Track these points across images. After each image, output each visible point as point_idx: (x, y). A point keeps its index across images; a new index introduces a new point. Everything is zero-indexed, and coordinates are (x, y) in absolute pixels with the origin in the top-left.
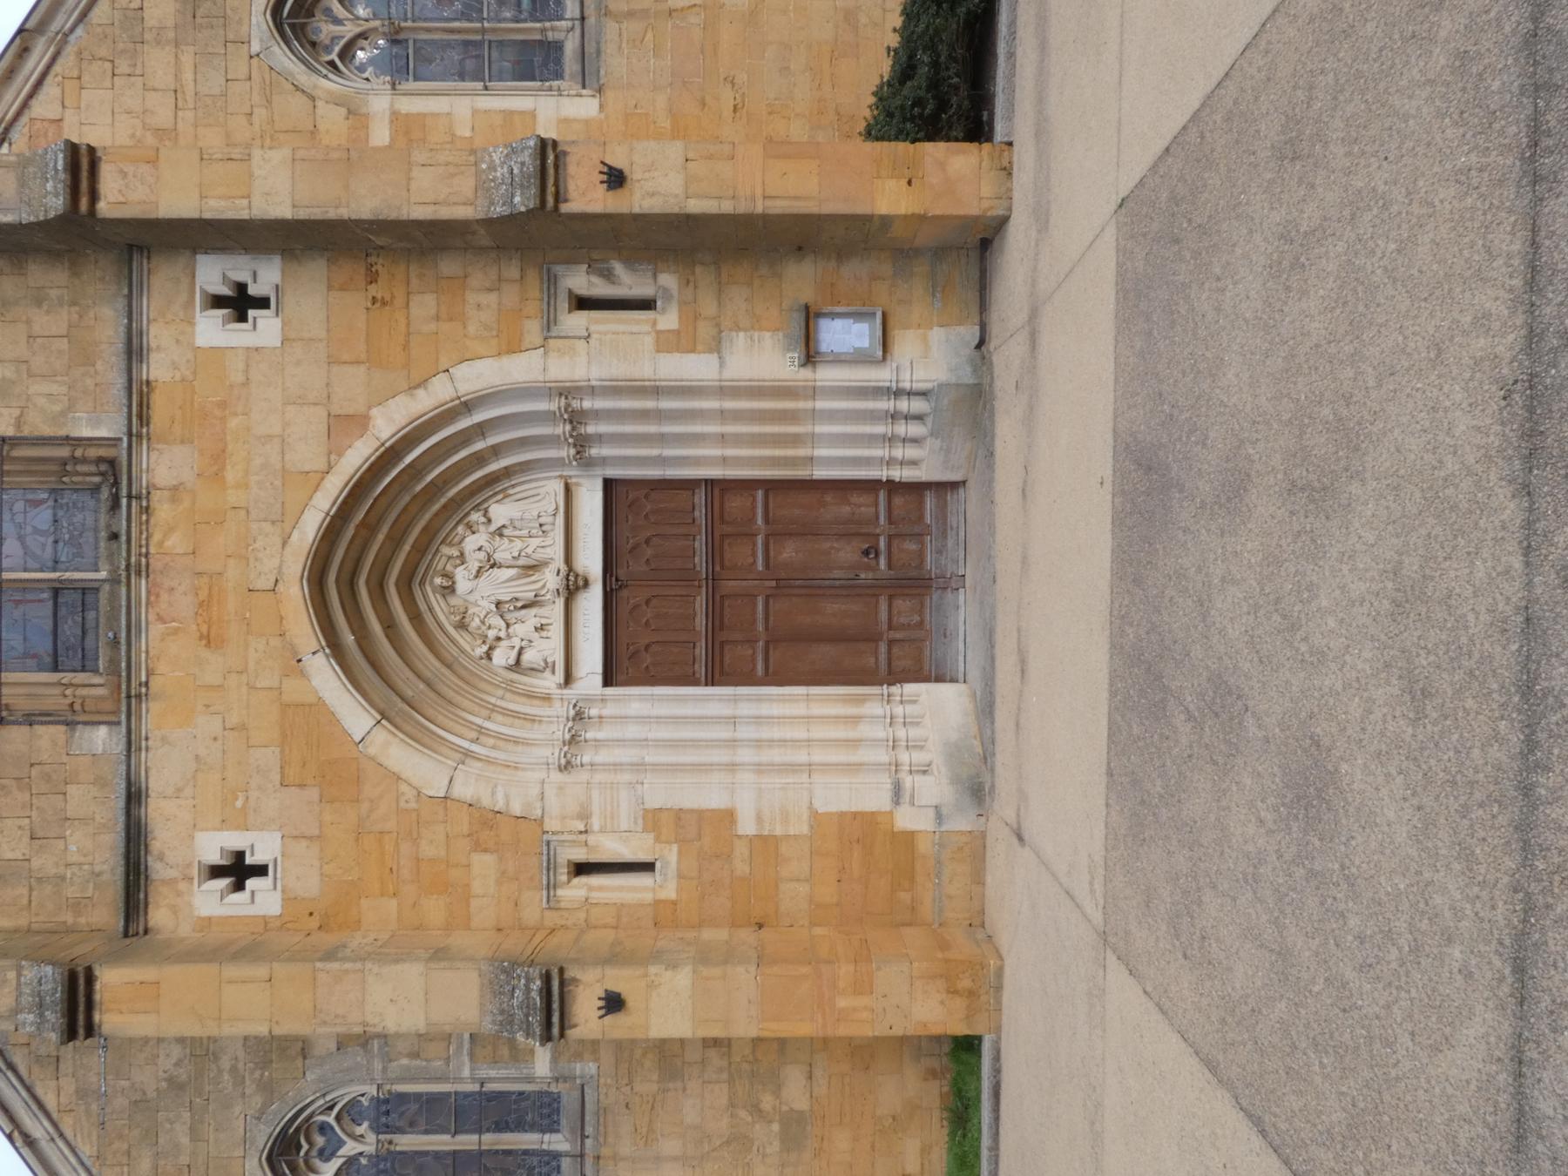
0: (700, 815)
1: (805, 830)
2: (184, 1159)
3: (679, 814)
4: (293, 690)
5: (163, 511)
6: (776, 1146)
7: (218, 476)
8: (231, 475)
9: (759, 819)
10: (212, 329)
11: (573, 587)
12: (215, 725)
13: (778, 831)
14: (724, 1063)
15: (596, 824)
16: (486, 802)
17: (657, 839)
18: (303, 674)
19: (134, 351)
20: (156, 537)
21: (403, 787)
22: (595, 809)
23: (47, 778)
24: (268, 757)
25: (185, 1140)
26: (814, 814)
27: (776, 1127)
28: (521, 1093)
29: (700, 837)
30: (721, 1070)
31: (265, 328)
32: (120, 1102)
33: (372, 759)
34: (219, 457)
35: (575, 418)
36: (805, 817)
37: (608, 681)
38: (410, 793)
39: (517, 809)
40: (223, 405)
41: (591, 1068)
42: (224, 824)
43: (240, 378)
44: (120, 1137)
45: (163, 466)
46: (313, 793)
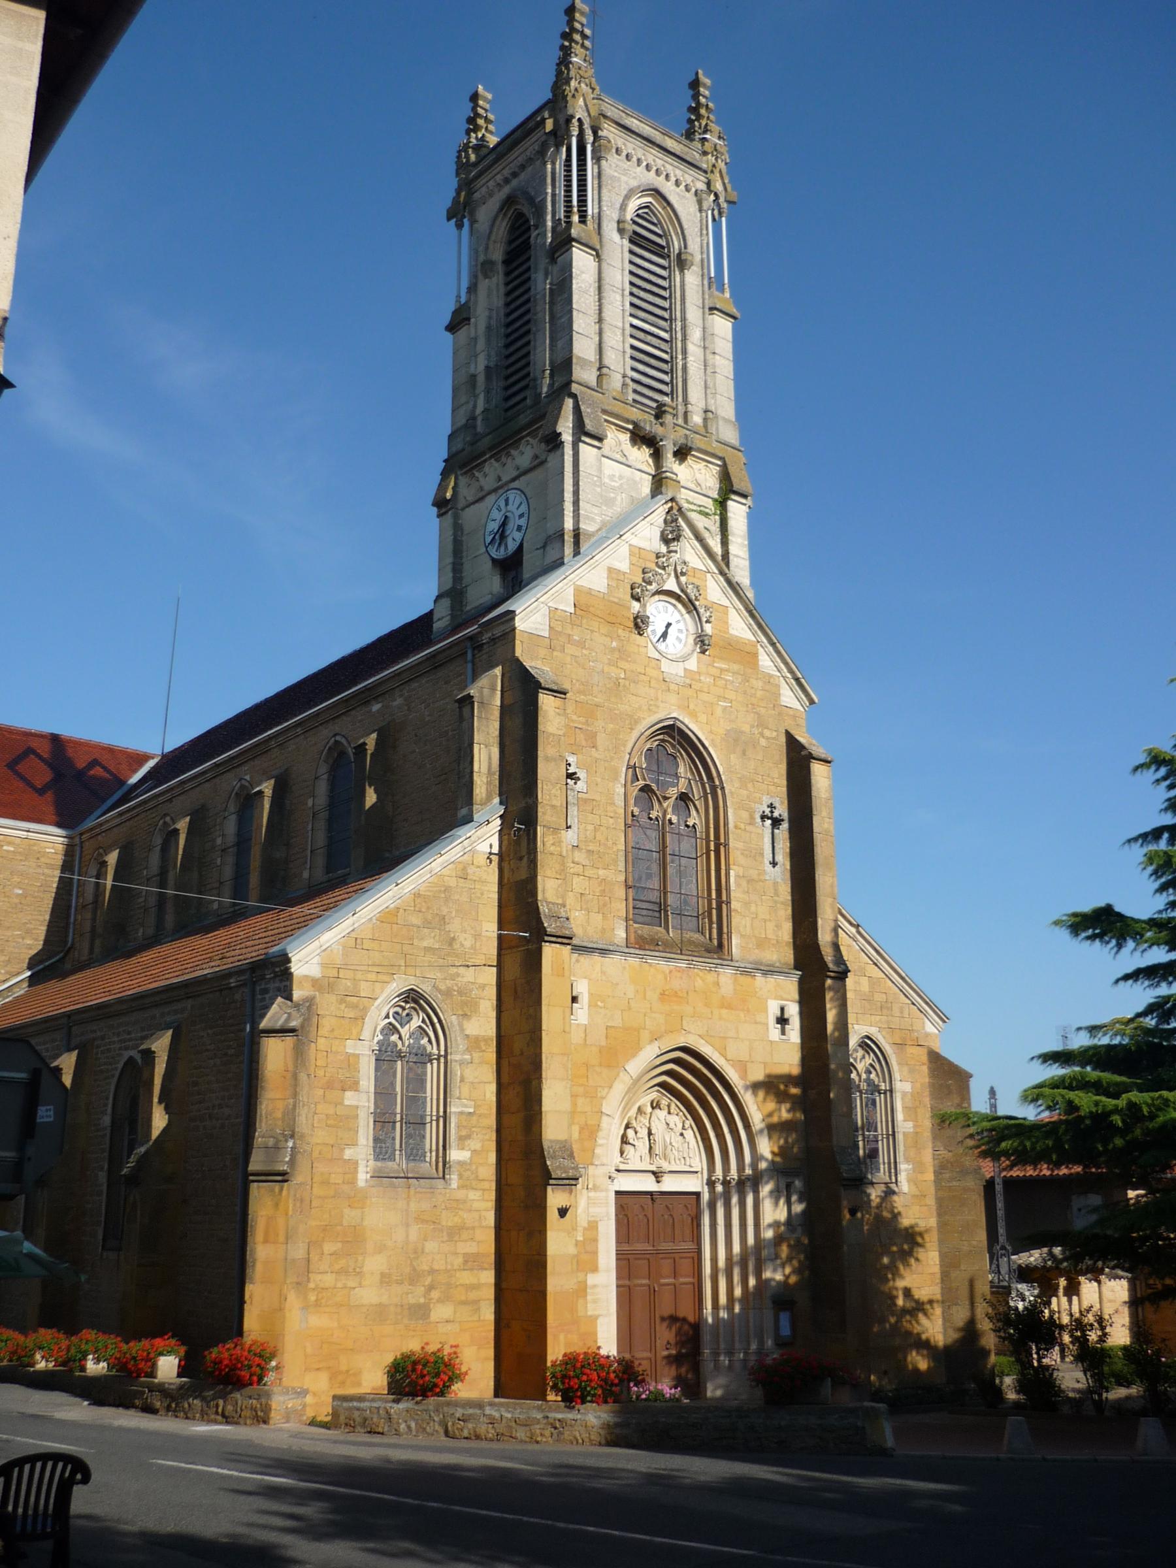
0: (595, 1253)
1: (589, 1313)
2: (416, 942)
3: (595, 1240)
4: (645, 1035)
5: (710, 977)
6: (412, 1301)
7: (722, 1006)
8: (724, 1012)
9: (595, 1286)
10: (773, 1010)
11: (657, 1175)
12: (630, 995)
13: (589, 1298)
14: (456, 1267)
15: (592, 1194)
16: (600, 1134)
17: (585, 1229)
18: (651, 1041)
19: (768, 971)
20: (701, 974)
21: (606, 1090)
22: (598, 1194)
23: (605, 905)
24: (617, 1022)
25: (425, 944)
26: (596, 1318)
27: (422, 1300)
28: (424, 1137)
29: (586, 1252)
30: (452, 1265)
31: (774, 1032)
32: (445, 911)
33: (618, 1075)
34: (729, 1007)
35: (741, 1183)
36: (596, 1313)
37: (618, 1193)
38: (604, 1093)
39: (597, 1151)
40: (748, 1011)
41: (454, 1185)
42: (591, 995)
43: (758, 1020)
44: (428, 908)
45: (726, 976)
46: (603, 1043)
